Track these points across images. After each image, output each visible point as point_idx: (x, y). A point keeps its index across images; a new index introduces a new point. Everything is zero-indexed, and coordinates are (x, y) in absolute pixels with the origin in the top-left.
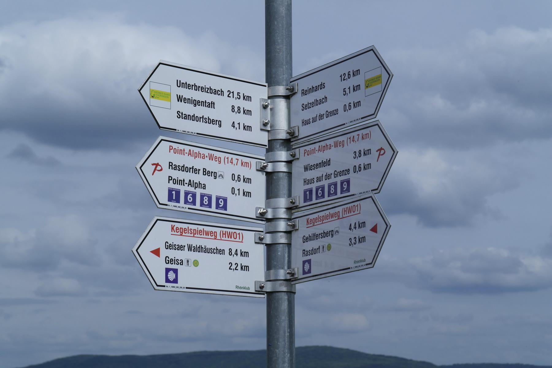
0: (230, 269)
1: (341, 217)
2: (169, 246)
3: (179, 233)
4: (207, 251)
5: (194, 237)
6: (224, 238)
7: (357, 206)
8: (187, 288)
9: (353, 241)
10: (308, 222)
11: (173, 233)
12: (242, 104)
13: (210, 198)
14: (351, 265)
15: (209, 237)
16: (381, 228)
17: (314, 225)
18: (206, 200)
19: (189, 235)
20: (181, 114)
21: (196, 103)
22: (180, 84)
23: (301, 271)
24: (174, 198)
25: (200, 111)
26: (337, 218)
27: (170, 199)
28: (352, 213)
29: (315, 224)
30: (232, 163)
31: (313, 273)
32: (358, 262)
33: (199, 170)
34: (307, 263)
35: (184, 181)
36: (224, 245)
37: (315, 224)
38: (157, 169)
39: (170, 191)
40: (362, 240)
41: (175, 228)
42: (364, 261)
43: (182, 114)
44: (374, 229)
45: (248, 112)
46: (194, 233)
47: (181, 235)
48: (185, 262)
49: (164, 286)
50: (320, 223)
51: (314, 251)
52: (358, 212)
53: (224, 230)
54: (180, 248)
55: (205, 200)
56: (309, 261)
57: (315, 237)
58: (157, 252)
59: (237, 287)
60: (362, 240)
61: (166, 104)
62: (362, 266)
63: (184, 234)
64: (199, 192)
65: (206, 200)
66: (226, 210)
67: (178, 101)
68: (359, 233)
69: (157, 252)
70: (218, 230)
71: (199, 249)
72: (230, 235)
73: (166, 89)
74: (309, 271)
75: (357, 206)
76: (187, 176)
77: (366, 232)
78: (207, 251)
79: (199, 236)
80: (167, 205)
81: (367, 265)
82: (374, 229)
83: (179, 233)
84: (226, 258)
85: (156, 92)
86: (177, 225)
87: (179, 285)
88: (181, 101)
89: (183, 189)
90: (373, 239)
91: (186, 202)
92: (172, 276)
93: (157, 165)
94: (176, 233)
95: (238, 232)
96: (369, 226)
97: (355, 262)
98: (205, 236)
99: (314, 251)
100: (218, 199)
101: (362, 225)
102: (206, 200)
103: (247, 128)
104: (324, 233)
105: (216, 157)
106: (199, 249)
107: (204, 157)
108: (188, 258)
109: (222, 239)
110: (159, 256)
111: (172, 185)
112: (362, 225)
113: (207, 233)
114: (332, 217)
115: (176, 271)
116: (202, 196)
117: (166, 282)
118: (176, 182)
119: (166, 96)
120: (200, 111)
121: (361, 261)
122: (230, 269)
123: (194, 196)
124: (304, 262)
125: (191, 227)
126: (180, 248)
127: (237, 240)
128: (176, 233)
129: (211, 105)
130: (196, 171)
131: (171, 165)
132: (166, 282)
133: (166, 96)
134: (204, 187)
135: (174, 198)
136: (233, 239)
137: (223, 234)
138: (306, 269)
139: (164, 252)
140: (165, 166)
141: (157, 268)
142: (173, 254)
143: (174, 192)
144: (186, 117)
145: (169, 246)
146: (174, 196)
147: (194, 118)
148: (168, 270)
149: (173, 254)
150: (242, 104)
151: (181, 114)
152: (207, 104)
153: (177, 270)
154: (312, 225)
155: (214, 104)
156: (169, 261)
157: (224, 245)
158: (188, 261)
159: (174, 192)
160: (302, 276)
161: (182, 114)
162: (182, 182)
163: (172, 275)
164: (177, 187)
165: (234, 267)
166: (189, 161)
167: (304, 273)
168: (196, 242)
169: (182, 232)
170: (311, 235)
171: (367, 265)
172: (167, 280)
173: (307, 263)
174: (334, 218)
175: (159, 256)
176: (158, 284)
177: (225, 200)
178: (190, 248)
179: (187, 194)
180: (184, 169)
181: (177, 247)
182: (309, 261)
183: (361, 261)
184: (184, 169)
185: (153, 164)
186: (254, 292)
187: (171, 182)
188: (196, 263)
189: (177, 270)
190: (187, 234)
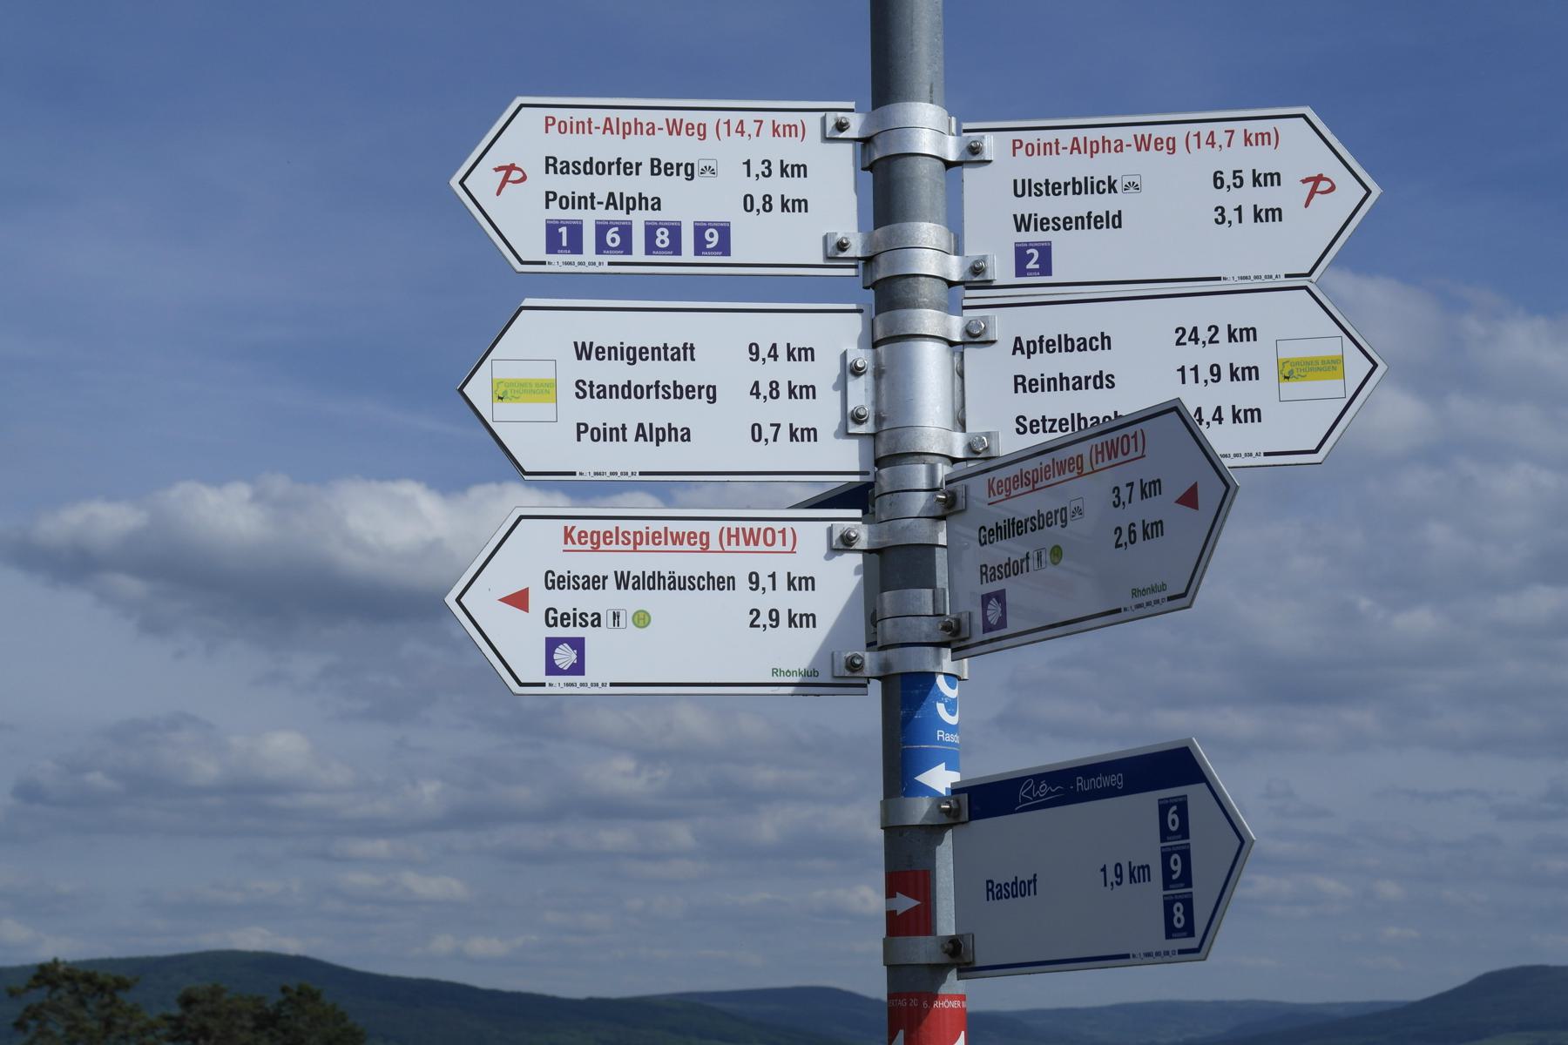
0: (752, 625)
1: (1087, 468)
2: (555, 582)
3: (588, 546)
4: (676, 583)
5: (635, 550)
6: (733, 547)
7: (1135, 436)
8: (612, 685)
9: (1124, 496)
10: (990, 488)
11: (570, 546)
12: (786, 372)
13: (675, 230)
14: (1125, 600)
15: (686, 546)
16: (1209, 495)
17: (1008, 497)
18: (665, 237)
19: (621, 547)
20: (587, 388)
21: (634, 355)
22: (583, 351)
23: (978, 620)
24: (564, 243)
25: (644, 373)
26: (1075, 474)
27: (553, 245)
28: (1121, 458)
29: (1014, 493)
30: (742, 133)
31: (1013, 625)
32: (1144, 592)
33: (638, 165)
34: (993, 601)
35: (592, 196)
36: (735, 564)
37: (1014, 493)
38: (511, 178)
39: (552, 229)
40: (1153, 529)
41: (575, 535)
42: (1163, 587)
43: (591, 385)
44: (1190, 499)
45: (809, 391)
46: (636, 542)
47: (595, 550)
48: (607, 619)
49: (543, 685)
50: (1025, 489)
51: (1013, 568)
52: (1139, 454)
53: (733, 525)
54: (594, 583)
55: (660, 237)
56: (1000, 596)
57: (1014, 528)
58: (519, 600)
59: (775, 672)
60: (1153, 529)
61: (545, 410)
62: (1157, 602)
63: (603, 547)
64: (639, 219)
65: (663, 238)
66: (727, 253)
67: (579, 357)
68: (1141, 511)
69: (519, 600)
70: (714, 528)
71: (653, 581)
72: (752, 538)
73: (544, 372)
74: (1002, 623)
75: (1135, 436)
76: (600, 186)
77: (1163, 507)
78: (676, 583)
79: (651, 547)
80: (543, 263)
81: (1170, 599)
82: (1190, 499)
83: (588, 546)
84: (743, 598)
85: (511, 384)
86: (581, 525)
87: (588, 677)
88: (588, 358)
89: (589, 219)
90: (1184, 527)
91: (601, 247)
92: (565, 656)
93: (511, 168)
94: (578, 547)
95: (778, 526)
96: (1174, 488)
97: (1135, 592)
98: (670, 546)
99: (1013, 568)
100: (700, 230)
101: (1151, 488)
102: (663, 238)
103: (810, 434)
104: (1040, 515)
105: (690, 127)
106: (653, 581)
107: (652, 130)
108: (616, 607)
109: (727, 548)
110: (526, 610)
111: (555, 212)
112: (1151, 488)
113: (677, 539)
114: (1061, 471)
115: (578, 644)
116: (651, 230)
117: (548, 673)
118: (566, 202)
119: (544, 390)
120: (644, 373)
121: (1153, 590)
122: (752, 625)
123: (625, 231)
124: (986, 599)
125: (624, 525)
126: (594, 583)
127: (778, 546)
128: (578, 547)
129: (686, 352)
130: (629, 168)
131: (550, 163)
132: (548, 673)
133: (544, 390)
134: (657, 204)
135: (564, 243)
136: (762, 546)
137: (730, 536)
138: (993, 618)
139: (541, 599)
140: (534, 167)
141: (521, 644)
142: (566, 601)
143: (563, 230)
144: (604, 392)
145: (555, 582)
146: (562, 238)
147: (629, 391)
148: (552, 644)
149: (566, 601)
150: (786, 372)
151: (587, 388)
152: (670, 353)
153: (582, 640)
154: (1003, 496)
155: (692, 348)
156: (552, 617)
157: (735, 564)
158: (616, 616)
159: (563, 230)
160: (979, 636)
161: (591, 385)
162: (588, 201)
163: (566, 651)
164: (571, 214)
165: (764, 619)
166: (605, 148)
167: (987, 628)
168: (638, 564)
169: (597, 543)
170: (1001, 524)
171: (1170, 599)
172: (552, 669)
173: (993, 601)
174: (1068, 475)
175: (526, 610)
176: (524, 312)
177: (724, 231)
178: (622, 581)
179: (602, 229)
180: (591, 167)
181: (581, 582)
182: (1000, 596)
183: (1153, 590)
184: (591, 167)
185: (498, 169)
186: (829, 680)
187: (554, 205)
188: (642, 619)
189: (582, 640)
190: (613, 547)
